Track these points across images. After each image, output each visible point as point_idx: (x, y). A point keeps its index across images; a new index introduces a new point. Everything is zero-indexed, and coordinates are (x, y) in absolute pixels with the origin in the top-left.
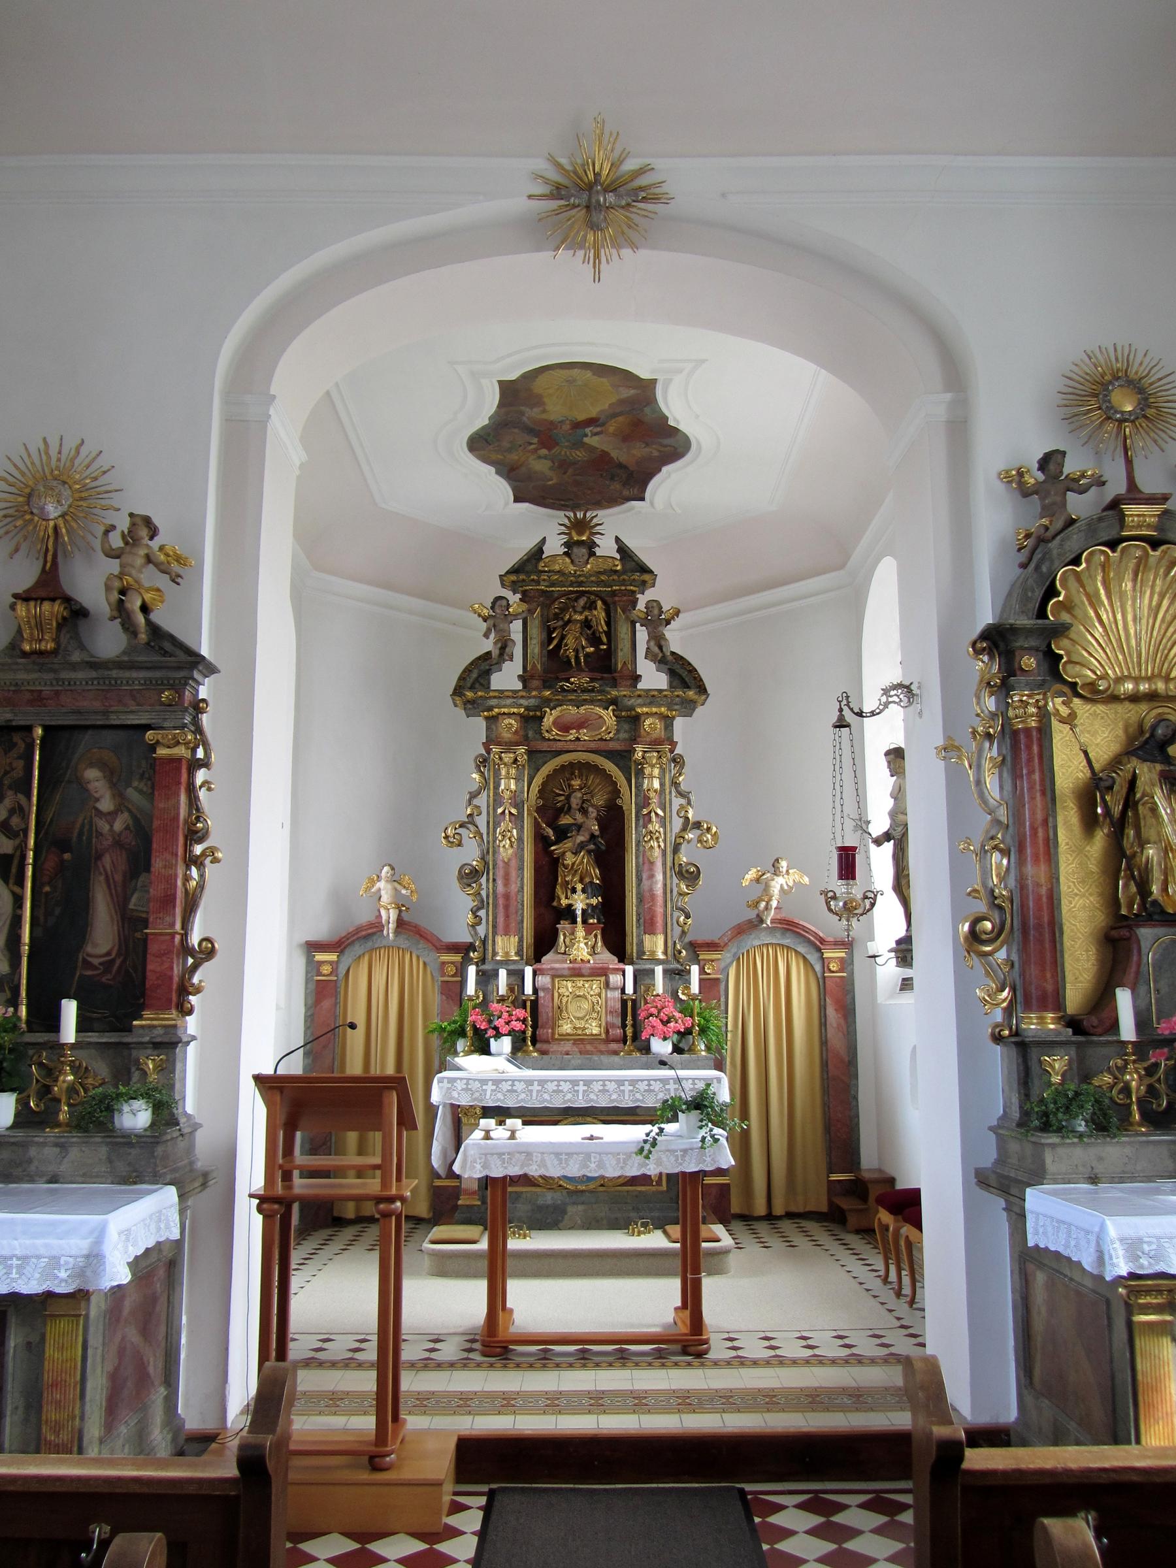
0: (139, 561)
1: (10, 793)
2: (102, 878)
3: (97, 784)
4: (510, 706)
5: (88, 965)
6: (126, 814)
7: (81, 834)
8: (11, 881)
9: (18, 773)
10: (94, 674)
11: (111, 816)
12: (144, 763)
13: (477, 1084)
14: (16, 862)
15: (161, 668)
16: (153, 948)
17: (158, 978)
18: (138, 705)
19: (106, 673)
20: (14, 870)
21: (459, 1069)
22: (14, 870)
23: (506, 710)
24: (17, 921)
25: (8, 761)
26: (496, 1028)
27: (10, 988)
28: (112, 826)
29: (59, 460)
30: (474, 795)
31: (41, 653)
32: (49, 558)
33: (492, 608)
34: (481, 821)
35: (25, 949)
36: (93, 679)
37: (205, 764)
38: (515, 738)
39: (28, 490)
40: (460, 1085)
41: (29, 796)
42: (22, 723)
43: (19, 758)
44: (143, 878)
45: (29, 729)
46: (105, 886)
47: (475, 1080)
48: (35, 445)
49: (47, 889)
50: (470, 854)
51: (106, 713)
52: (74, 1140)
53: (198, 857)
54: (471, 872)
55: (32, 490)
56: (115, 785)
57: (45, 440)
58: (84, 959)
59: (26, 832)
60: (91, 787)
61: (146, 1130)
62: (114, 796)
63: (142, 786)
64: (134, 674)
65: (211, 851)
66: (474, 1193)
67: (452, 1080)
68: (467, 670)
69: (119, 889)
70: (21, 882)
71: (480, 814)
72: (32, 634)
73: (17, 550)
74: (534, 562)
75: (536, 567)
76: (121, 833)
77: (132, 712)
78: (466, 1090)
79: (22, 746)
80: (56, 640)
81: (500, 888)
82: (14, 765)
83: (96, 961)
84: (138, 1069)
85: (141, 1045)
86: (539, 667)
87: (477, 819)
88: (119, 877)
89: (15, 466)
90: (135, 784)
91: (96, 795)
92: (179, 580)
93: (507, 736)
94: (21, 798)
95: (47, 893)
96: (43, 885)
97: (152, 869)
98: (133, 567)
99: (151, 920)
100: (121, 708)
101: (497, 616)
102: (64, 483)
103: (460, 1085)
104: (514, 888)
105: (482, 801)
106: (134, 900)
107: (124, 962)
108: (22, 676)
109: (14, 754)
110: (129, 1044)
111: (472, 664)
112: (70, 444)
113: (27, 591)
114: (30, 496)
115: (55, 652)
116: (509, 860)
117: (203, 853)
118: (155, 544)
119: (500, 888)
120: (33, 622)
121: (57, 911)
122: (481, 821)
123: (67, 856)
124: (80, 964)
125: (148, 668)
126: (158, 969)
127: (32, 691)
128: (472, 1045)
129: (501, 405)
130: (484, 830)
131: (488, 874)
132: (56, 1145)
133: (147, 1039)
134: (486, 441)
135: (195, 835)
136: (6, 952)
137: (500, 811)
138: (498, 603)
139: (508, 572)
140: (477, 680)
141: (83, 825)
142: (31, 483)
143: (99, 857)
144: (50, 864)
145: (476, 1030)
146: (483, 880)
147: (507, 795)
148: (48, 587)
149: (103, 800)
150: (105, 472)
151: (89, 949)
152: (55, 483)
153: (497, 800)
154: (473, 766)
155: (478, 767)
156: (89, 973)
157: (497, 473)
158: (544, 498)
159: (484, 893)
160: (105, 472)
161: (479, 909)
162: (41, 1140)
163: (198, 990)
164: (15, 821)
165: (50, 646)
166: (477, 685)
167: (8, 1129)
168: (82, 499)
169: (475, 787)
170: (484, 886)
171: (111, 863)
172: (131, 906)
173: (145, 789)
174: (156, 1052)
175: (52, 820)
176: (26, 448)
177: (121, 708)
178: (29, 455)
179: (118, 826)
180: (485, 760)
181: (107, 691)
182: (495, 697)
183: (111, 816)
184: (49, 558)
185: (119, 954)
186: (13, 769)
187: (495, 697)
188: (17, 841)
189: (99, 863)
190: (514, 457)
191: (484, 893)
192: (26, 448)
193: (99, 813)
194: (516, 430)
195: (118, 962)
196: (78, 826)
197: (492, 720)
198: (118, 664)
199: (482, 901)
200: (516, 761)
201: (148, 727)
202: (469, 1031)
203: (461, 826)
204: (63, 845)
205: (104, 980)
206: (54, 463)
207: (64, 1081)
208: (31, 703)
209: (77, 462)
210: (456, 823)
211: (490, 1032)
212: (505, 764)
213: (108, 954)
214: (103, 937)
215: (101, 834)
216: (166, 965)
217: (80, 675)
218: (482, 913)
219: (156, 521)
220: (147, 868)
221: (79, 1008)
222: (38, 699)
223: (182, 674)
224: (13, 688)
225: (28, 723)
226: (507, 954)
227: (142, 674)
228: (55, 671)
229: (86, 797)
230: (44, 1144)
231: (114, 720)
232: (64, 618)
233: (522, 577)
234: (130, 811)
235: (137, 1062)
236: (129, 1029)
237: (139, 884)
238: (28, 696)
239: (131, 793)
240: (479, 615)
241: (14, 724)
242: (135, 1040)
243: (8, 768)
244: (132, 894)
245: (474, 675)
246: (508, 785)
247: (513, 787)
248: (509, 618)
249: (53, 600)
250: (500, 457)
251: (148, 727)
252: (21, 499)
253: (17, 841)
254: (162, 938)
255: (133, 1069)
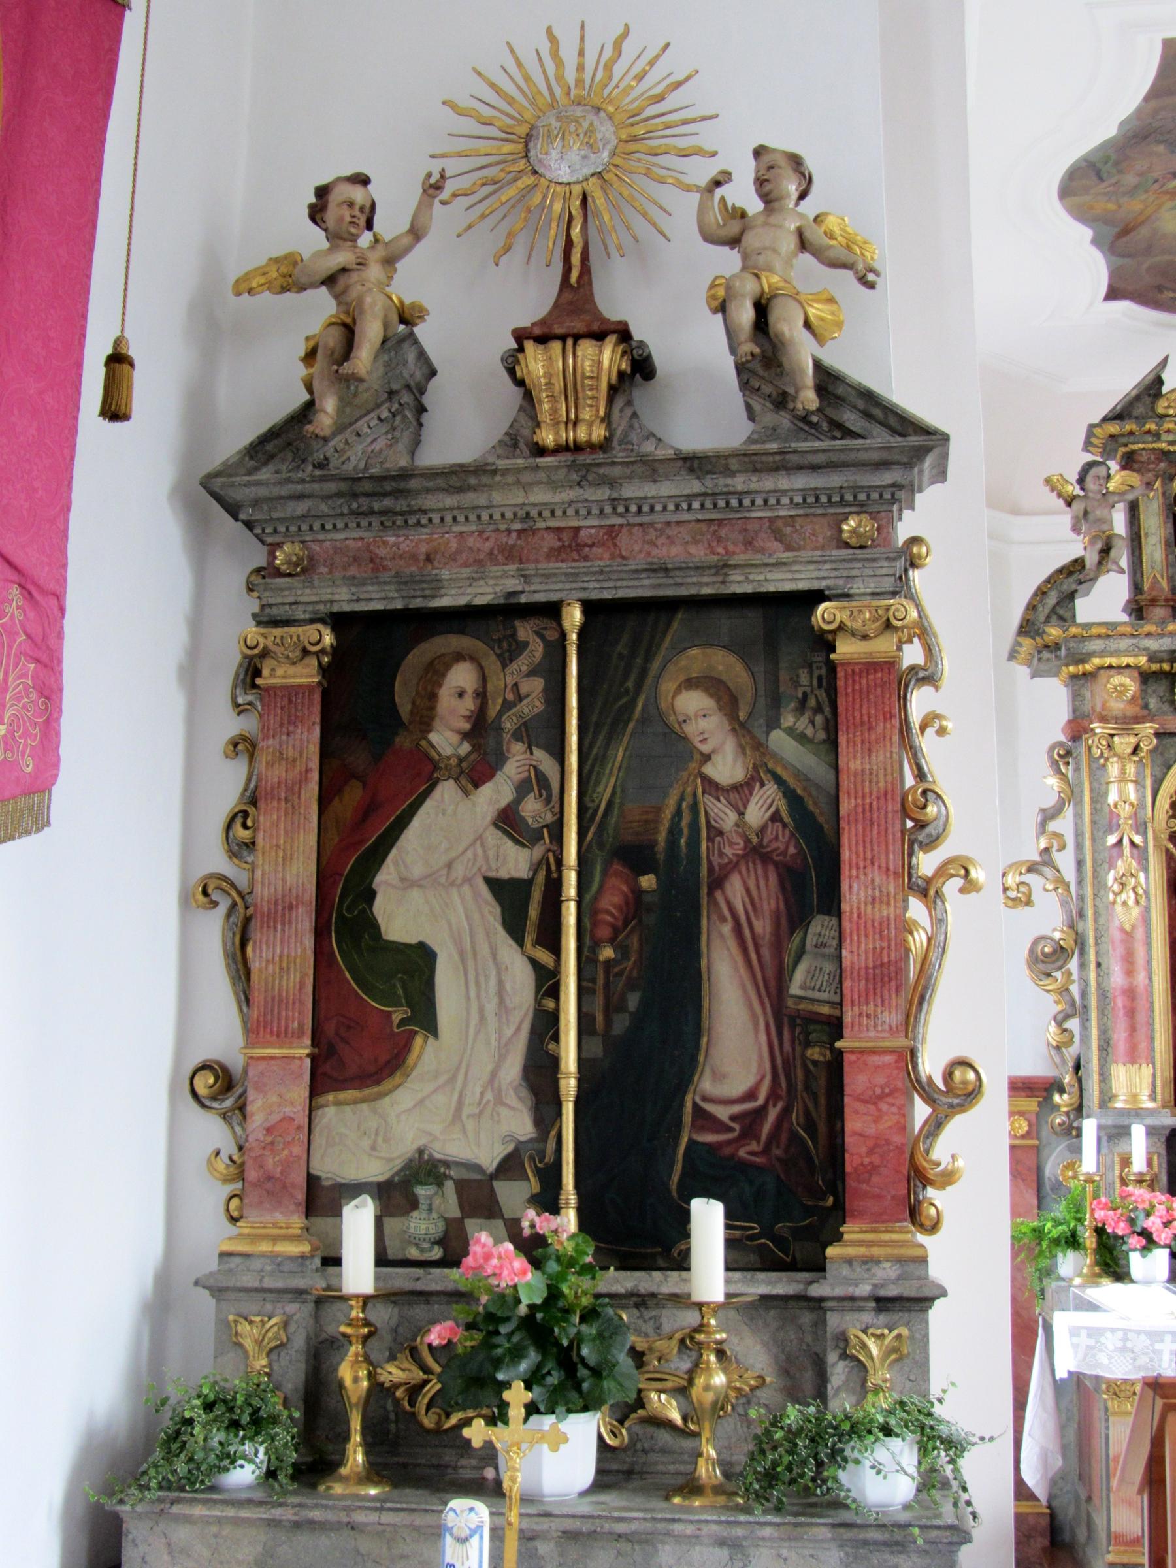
0: (789, 243)
1: (518, 748)
2: (727, 929)
3: (703, 724)
4: (1127, 653)
5: (703, 1118)
6: (771, 789)
7: (674, 832)
8: (529, 940)
9: (534, 703)
10: (696, 486)
11: (740, 792)
12: (804, 677)
13: (1144, 1341)
14: (537, 895)
15: (845, 465)
16: (856, 1082)
17: (871, 1152)
18: (789, 548)
19: (722, 481)
20: (533, 913)
21: (1093, 1307)
22: (533, 913)
23: (1113, 661)
24: (545, 1025)
25: (510, 680)
26: (1145, 1234)
27: (539, 1173)
28: (741, 814)
29: (580, 68)
30: (1049, 815)
31: (578, 448)
32: (576, 259)
33: (1081, 481)
34: (1065, 861)
35: (569, 1086)
36: (690, 497)
37: (927, 677)
38: (1133, 710)
39: (523, 130)
40: (1111, 1342)
41: (560, 756)
42: (541, 597)
43: (532, 673)
44: (820, 927)
45: (553, 611)
46: (732, 943)
47: (1138, 1332)
48: (531, 42)
49: (607, 953)
50: (1047, 918)
51: (722, 568)
52: (767, 1531)
53: (928, 881)
54: (1054, 952)
55: (532, 128)
56: (742, 725)
57: (549, 31)
58: (695, 1105)
59: (557, 831)
60: (690, 730)
61: (906, 1507)
62: (742, 748)
63: (802, 724)
64: (784, 482)
65: (961, 867)
66: (1137, 1541)
67: (1095, 1333)
68: (1041, 593)
69: (766, 953)
70: (553, 944)
71: (1062, 847)
72: (554, 411)
73: (507, 249)
74: (1147, 400)
75: (1153, 409)
76: (763, 829)
77: (779, 564)
78: (1124, 1349)
79: (537, 650)
80: (607, 419)
81: (1117, 978)
82: (524, 688)
83: (723, 1113)
84: (844, 1356)
85: (850, 1302)
86: (1164, 584)
87: (1057, 857)
88: (763, 926)
89: (493, 86)
90: (788, 720)
91: (705, 748)
92: (871, 277)
93: (1117, 706)
94: (545, 761)
95: (608, 963)
96: (597, 944)
97: (845, 907)
98: (775, 251)
99: (847, 1019)
100: (758, 558)
101: (1081, 499)
102: (598, 109)
103: (1111, 1342)
104: (1141, 978)
105: (1064, 825)
106: (799, 975)
107: (786, 1112)
108: (540, 496)
109: (522, 664)
110: (822, 1299)
111: (1048, 581)
112: (600, 38)
113: (542, 322)
114: (528, 138)
115: (604, 446)
116: (1133, 927)
117: (943, 872)
118: (809, 207)
119: (1117, 978)
120: (558, 385)
121: (633, 1001)
122: (1065, 861)
123: (647, 882)
124: (687, 1118)
125: (814, 468)
126: (871, 1130)
127: (559, 530)
128: (1097, 1263)
129: (1154, 93)
130: (1070, 875)
131: (1082, 953)
132: (722, 1543)
133: (864, 1289)
134: (1098, 174)
135: (922, 832)
136: (524, 1093)
137: (1112, 840)
138: (1093, 471)
139: (1105, 420)
140: (1053, 610)
141: (678, 813)
142: (528, 116)
143: (717, 883)
144: (611, 901)
145: (1100, 1231)
146: (1073, 965)
147: (1125, 811)
148: (575, 316)
149: (717, 758)
150: (679, 84)
151: (706, 1084)
152: (579, 111)
153: (1104, 820)
154: (1045, 762)
155: (1055, 765)
156: (710, 1138)
157: (1096, 242)
158: (1160, 288)
159: (1075, 989)
160: (679, 84)
161: (1067, 1017)
162: (689, 1530)
163: (948, 1178)
164: (532, 808)
165: (599, 433)
166: (1054, 619)
167: (583, 1494)
168: (635, 139)
169: (1050, 801)
170: (1075, 976)
171: (747, 894)
172: (795, 989)
173: (809, 732)
174: (883, 1318)
175: (610, 804)
176: (512, 51)
177: (758, 558)
178: (519, 64)
179: (756, 814)
180: (1068, 753)
181: (720, 522)
182: (1099, 636)
183: (740, 792)
184: (576, 259)
185: (773, 1095)
186: (521, 699)
187: (1099, 636)
188: (538, 851)
189: (718, 895)
190: (1135, 206)
191: (1075, 989)
192: (512, 51)
193: (711, 786)
194: (1161, 148)
195: (773, 1114)
196: (668, 814)
197: (1082, 680)
198: (750, 461)
199: (1073, 1004)
200: (1136, 750)
201: (818, 596)
202: (1088, 1238)
203: (1029, 870)
204: (636, 856)
205: (742, 1153)
206: (570, 76)
207: (707, 1388)
208: (556, 553)
209: (618, 70)
210: (1022, 863)
211: (1135, 1241)
212: (1119, 757)
213: (751, 1095)
214: (735, 1060)
215: (720, 833)
216: (887, 1122)
217: (666, 489)
218: (1073, 1024)
219: (811, 164)
220: (831, 903)
221: (729, 1215)
222: (571, 544)
223: (887, 477)
224: (517, 526)
225: (554, 597)
226: (1134, 1097)
227: (801, 481)
228: (612, 483)
229: (677, 749)
230: (695, 1539)
231: (739, 584)
232: (621, 374)
233: (1130, 426)
234: (778, 779)
235: (842, 1339)
236: (818, 1266)
237: (810, 941)
238: (550, 541)
239: (779, 741)
240: (1060, 495)
241: (523, 599)
242: (838, 1291)
243: (510, 697)
244: (796, 963)
245: (1052, 599)
246: (1123, 790)
247: (1133, 797)
248: (1112, 499)
249: (599, 336)
250: (1111, 206)
251: (818, 596)
252: (507, 148)
253: (538, 851)
254: (876, 1059)
255: (832, 1357)
